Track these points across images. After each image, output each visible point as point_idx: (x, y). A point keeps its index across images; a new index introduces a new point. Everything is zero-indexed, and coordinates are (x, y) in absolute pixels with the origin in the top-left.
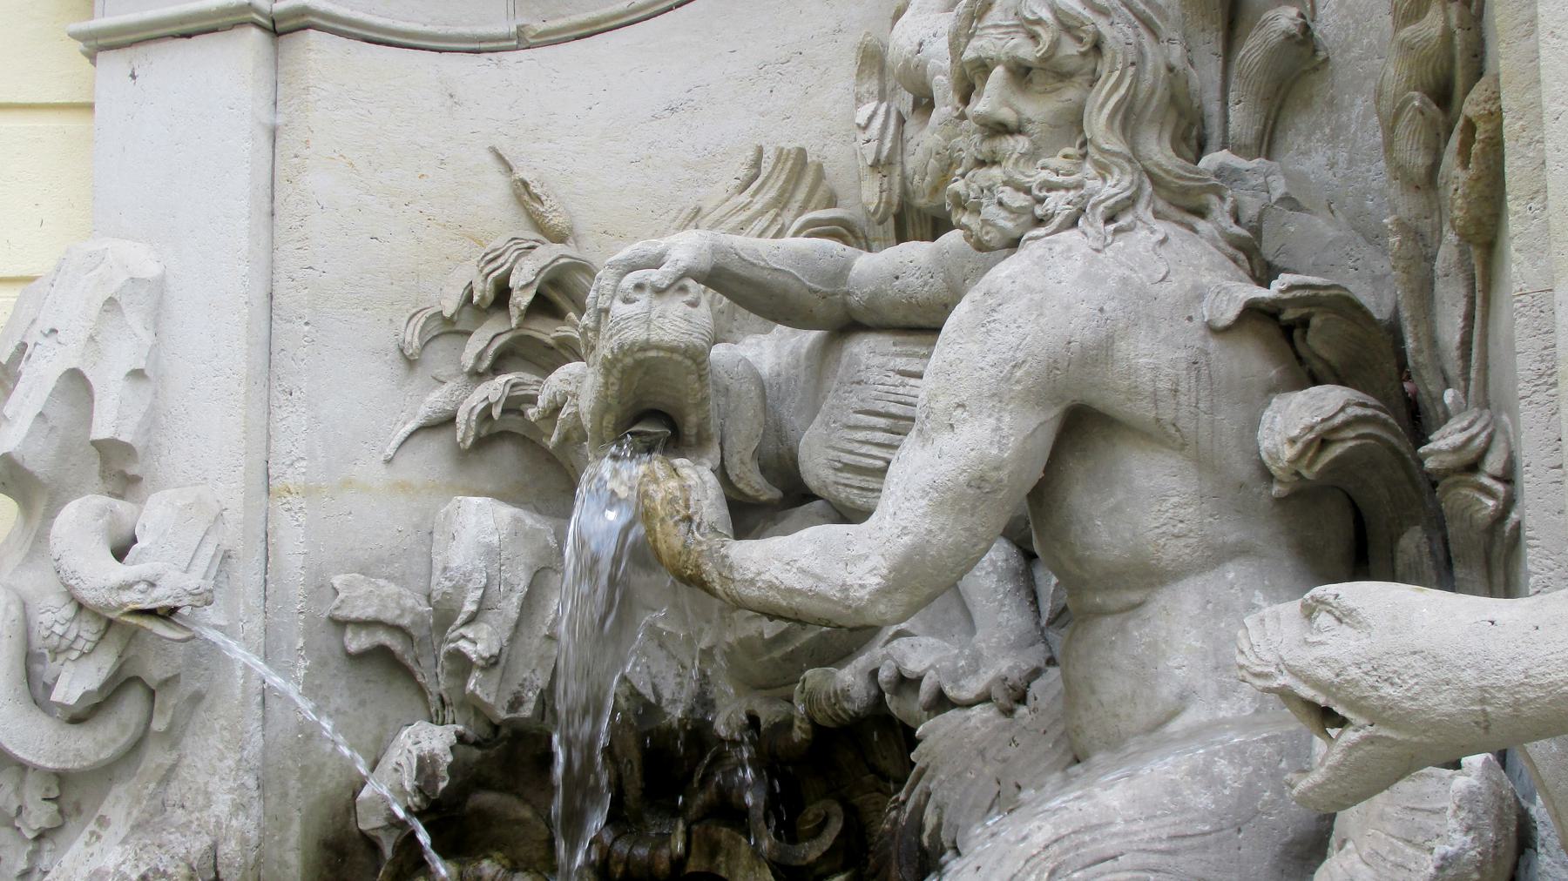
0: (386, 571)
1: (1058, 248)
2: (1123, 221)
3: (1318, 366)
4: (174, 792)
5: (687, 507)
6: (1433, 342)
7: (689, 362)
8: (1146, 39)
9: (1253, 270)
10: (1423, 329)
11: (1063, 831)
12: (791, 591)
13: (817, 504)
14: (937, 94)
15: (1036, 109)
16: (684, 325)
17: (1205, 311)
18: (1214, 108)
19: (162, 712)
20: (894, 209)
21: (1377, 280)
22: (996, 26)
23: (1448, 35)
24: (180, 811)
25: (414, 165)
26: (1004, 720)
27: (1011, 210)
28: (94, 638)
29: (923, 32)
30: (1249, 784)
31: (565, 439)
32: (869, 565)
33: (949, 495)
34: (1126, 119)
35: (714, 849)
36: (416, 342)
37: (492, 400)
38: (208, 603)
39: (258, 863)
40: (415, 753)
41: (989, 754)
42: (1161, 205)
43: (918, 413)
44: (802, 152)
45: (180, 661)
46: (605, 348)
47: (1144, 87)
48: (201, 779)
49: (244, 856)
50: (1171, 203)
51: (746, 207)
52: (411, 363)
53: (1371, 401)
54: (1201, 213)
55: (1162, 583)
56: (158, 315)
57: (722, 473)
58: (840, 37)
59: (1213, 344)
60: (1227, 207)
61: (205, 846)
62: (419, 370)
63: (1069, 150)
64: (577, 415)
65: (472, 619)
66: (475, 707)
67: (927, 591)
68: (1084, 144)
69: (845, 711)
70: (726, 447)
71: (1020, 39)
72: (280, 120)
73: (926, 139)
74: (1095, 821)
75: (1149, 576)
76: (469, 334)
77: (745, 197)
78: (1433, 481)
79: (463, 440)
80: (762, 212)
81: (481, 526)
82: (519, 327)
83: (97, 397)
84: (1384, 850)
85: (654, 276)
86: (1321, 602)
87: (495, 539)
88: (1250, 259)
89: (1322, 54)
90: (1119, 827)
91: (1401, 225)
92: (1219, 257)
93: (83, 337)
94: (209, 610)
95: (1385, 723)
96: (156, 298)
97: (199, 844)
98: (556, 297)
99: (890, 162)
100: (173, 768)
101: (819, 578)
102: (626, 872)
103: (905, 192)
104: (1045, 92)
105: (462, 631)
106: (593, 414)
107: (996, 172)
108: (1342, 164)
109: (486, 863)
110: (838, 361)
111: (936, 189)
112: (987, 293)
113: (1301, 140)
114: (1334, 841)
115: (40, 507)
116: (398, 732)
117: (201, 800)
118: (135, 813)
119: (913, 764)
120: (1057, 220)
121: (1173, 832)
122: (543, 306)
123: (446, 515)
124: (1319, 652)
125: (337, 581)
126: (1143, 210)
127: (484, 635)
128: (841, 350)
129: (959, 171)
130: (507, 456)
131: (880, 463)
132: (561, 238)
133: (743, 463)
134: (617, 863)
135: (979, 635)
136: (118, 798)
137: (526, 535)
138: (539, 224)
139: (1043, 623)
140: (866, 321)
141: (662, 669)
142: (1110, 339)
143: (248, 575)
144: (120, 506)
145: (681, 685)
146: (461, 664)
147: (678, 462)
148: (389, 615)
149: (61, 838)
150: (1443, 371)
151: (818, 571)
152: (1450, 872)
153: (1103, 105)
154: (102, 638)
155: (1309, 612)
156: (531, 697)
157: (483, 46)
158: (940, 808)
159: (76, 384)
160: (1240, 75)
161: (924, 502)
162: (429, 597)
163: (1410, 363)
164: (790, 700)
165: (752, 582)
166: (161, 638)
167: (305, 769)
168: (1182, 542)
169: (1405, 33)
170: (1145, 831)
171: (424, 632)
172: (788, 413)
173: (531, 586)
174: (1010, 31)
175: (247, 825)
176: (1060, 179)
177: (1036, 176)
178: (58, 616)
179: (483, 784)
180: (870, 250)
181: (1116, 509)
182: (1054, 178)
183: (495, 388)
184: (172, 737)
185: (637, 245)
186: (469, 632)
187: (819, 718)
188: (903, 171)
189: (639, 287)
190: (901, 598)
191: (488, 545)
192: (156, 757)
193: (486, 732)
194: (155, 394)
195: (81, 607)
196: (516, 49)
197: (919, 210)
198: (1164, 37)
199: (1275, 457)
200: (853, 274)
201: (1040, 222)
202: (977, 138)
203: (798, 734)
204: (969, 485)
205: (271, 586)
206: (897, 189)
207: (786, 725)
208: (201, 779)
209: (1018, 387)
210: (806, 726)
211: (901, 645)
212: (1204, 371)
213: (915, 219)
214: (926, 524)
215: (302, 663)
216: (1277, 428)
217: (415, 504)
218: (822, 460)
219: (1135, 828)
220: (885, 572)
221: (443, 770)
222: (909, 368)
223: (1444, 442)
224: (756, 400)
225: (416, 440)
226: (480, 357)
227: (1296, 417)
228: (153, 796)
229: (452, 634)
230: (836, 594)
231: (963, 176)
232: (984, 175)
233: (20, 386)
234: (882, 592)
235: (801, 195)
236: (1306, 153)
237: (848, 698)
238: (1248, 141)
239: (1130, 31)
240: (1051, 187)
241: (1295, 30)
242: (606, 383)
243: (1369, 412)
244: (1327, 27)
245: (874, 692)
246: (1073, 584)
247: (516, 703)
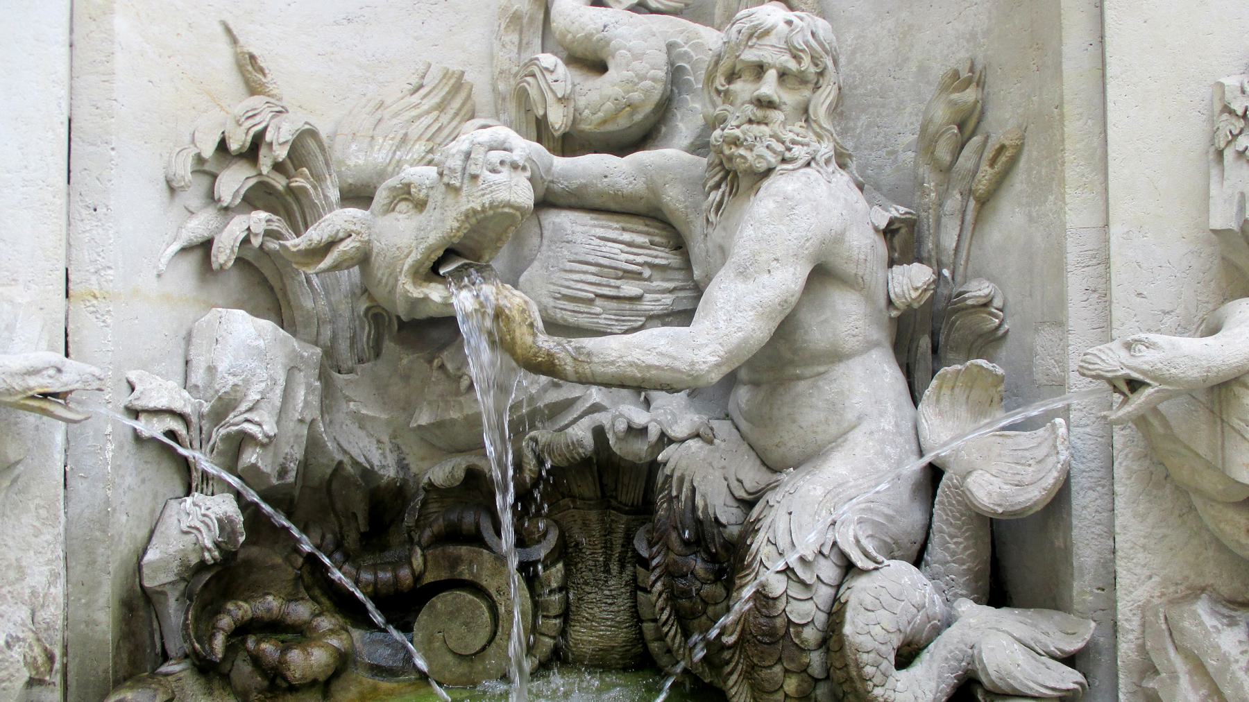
12: (649, 367)
15: (789, 98)
22: (773, 46)
32: (708, 350)
51: (417, 106)
52: (172, 190)
55: (840, 360)
69: (578, 454)
75: (836, 356)
77: (416, 98)
80: (428, 112)
101: (675, 358)
105: (247, 416)
117: (12, 575)
140: (561, 201)
156: (293, 466)
158: (704, 496)
165: (613, 363)
174: (781, 50)
181: (826, 321)
191: (258, 347)
201: (784, 161)
208: (12, 556)
218: (544, 292)
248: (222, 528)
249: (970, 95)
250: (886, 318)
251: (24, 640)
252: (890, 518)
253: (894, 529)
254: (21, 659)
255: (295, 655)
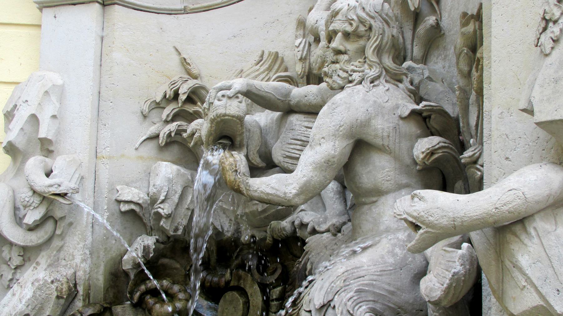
0: (134, 185)
1: (355, 91)
2: (376, 83)
3: (433, 130)
4: (62, 255)
5: (236, 167)
6: (468, 124)
7: (238, 121)
8: (386, 27)
9: (415, 99)
10: (465, 120)
11: (349, 269)
12: (268, 194)
13: (278, 168)
14: (322, 38)
15: (351, 46)
16: (237, 109)
17: (399, 112)
18: (409, 47)
19: (59, 228)
20: (306, 74)
21: (453, 104)
23: (475, 31)
24: (64, 261)
25: (147, 51)
26: (333, 237)
27: (342, 78)
28: (39, 203)
29: (317, 17)
30: (405, 256)
31: (196, 144)
32: (293, 186)
33: (318, 165)
34: (378, 51)
35: (239, 278)
36: (147, 110)
37: (172, 130)
38: (77, 192)
39: (89, 279)
40: (142, 245)
41: (329, 247)
42: (388, 78)
43: (310, 140)
44: (277, 53)
45: (66, 211)
46: (211, 115)
47: (384, 41)
48: (71, 251)
49: (85, 276)
50: (391, 78)
52: (145, 117)
53: (447, 141)
54: (400, 81)
55: (383, 195)
56: (61, 98)
57: (247, 157)
58: (291, 15)
59: (401, 122)
60: (409, 80)
61: (72, 272)
62: (148, 119)
63: (360, 60)
64: (200, 136)
65: (163, 202)
66: (163, 231)
67: (311, 195)
68: (365, 58)
69: (283, 234)
70: (249, 148)
71: (347, 24)
72: (104, 34)
73: (318, 51)
74: (358, 266)
76: (164, 108)
78: (465, 165)
79: (162, 143)
80: (263, 72)
81: (167, 171)
82: (181, 106)
83: (41, 123)
84: (440, 273)
85: (228, 93)
86: (415, 195)
87: (171, 176)
88: (415, 96)
89: (443, 32)
90: (366, 268)
91: (460, 88)
92: (405, 95)
93: (37, 103)
94: (76, 195)
95: (430, 227)
96: (61, 92)
97: (70, 272)
98: (194, 97)
99: (305, 59)
100: (62, 247)
101: (277, 190)
102: (211, 285)
103: (310, 68)
104: (354, 41)
105: (159, 205)
106: (206, 136)
107: (338, 66)
108: (447, 67)
109: (164, 281)
110: (286, 122)
111: (320, 68)
112: (333, 104)
113: (435, 59)
114: (428, 272)
115: (20, 160)
116: (137, 238)
117: (71, 257)
118: (49, 261)
119: (304, 250)
120: (356, 82)
121: (381, 269)
122: (190, 100)
123: (155, 167)
124: (414, 208)
125: (118, 188)
126: (382, 80)
127: (167, 207)
128: (287, 119)
129: (326, 64)
130: (175, 149)
131: (298, 156)
132: (196, 78)
133: (254, 154)
134: (208, 282)
135: (327, 211)
136: (43, 256)
137: (181, 175)
138: (189, 73)
139: (348, 208)
140: (296, 109)
141: (224, 220)
142: (370, 119)
143: (89, 184)
144: (47, 159)
145: (230, 226)
146: (158, 216)
147: (233, 152)
148: (135, 200)
149: (23, 269)
150: (471, 133)
151: (277, 188)
152: (456, 277)
153: (371, 47)
154: (41, 203)
155: (413, 198)
156: (181, 228)
157: (172, 12)
158: (312, 263)
159: (34, 118)
160: (417, 37)
161: (311, 167)
162: (148, 194)
163: (461, 130)
164: (266, 232)
165: (256, 191)
166: (61, 203)
167: (106, 249)
168: (389, 183)
169: (463, 30)
170: (373, 269)
171: (146, 205)
172: (270, 139)
173: (182, 192)
174: (344, 22)
175: (86, 266)
176: (357, 69)
177: (350, 68)
178: (27, 195)
179: (164, 256)
180: (298, 87)
182: (355, 69)
183: (173, 126)
184: (62, 236)
185: (223, 82)
186: (162, 206)
187: (275, 236)
188: (310, 62)
189: (223, 96)
190: (302, 197)
191: (169, 178)
192: (56, 243)
193: (165, 239)
194: (60, 123)
195: (34, 192)
196: (183, 14)
197: (314, 74)
198: (391, 26)
199: (418, 158)
200: (292, 94)
201: (351, 82)
202: (332, 54)
203: (269, 240)
204: (325, 163)
205: (96, 188)
206: (307, 67)
207: (265, 239)
208: (71, 251)
209: (341, 133)
210: (271, 239)
211: (303, 213)
212: (398, 131)
213: (313, 77)
214: (311, 174)
215: (106, 214)
216: (419, 148)
217: (144, 164)
219: (370, 268)
220: (298, 189)
221: (152, 250)
222: (309, 126)
223: (467, 154)
224: (259, 134)
225: (145, 142)
226: (168, 116)
227: (425, 145)
228: (55, 256)
229: (156, 206)
230: (282, 195)
231: (328, 66)
232: (334, 66)
233: (15, 119)
234: (297, 195)
235: (276, 67)
236: (436, 63)
237: (285, 231)
238: (419, 58)
239: (380, 24)
240: (354, 71)
241: (434, 24)
242: (211, 127)
243: (446, 145)
244: (444, 23)
245: (293, 229)
246: (357, 196)
247: (176, 230)
248: (144, 250)
249: (471, 28)
250: (414, 170)
251: (61, 281)
252: (392, 293)
253: (395, 299)
254: (55, 288)
255: (158, 306)
